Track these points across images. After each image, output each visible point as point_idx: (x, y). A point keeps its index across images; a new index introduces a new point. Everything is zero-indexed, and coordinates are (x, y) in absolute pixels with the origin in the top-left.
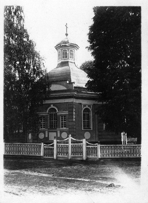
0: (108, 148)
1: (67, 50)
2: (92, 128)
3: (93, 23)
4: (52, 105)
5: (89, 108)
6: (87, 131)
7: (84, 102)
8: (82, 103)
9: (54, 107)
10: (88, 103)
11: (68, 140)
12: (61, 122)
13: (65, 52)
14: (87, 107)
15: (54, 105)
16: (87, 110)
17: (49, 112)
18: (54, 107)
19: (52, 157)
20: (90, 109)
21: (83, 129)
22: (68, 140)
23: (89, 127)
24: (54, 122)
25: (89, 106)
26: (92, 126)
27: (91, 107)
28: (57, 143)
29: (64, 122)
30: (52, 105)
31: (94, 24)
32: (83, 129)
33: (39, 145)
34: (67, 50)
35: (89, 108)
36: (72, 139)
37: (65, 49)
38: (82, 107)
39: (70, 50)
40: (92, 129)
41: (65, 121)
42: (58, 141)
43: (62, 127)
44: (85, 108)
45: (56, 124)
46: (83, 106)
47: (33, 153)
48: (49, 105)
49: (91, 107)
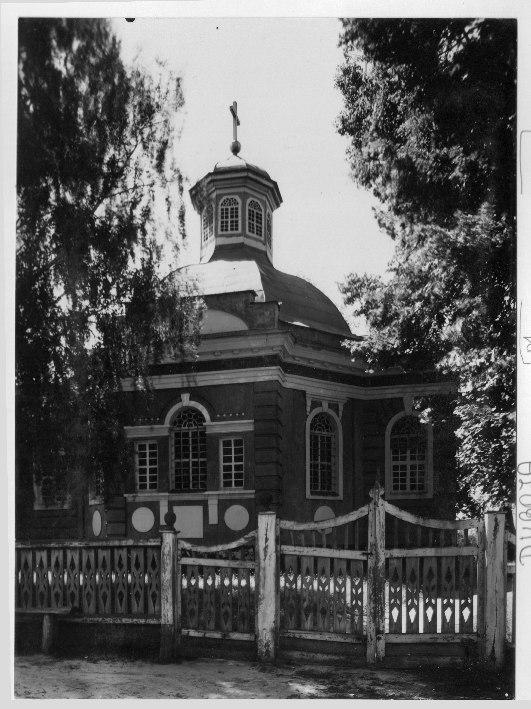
0: (142, 561)
1: (239, 200)
2: (341, 493)
3: (254, 262)
4: (185, 397)
5: (332, 413)
6: (324, 503)
7: (313, 388)
8: (310, 391)
9: (193, 404)
10: (330, 393)
11: (364, 521)
12: (222, 464)
13: (229, 208)
14: (325, 407)
15: (197, 393)
16: (323, 421)
17: (173, 423)
18: (193, 404)
19: (245, 637)
20: (338, 420)
21: (308, 495)
22: (364, 521)
23: (329, 488)
24: (195, 464)
25: (334, 406)
26: (341, 482)
27: (341, 408)
28: (283, 538)
29: (233, 464)
30: (185, 397)
31: (258, 263)
32: (308, 495)
33: (146, 548)
34: (239, 200)
35: (332, 413)
36: (389, 518)
37: (229, 194)
38: (308, 409)
39: (248, 201)
40: (341, 497)
41: (237, 459)
42: (288, 525)
43: (228, 484)
44: (317, 411)
45: (204, 471)
46: (309, 403)
47: (121, 609)
48: (174, 395)
49: (341, 408)
